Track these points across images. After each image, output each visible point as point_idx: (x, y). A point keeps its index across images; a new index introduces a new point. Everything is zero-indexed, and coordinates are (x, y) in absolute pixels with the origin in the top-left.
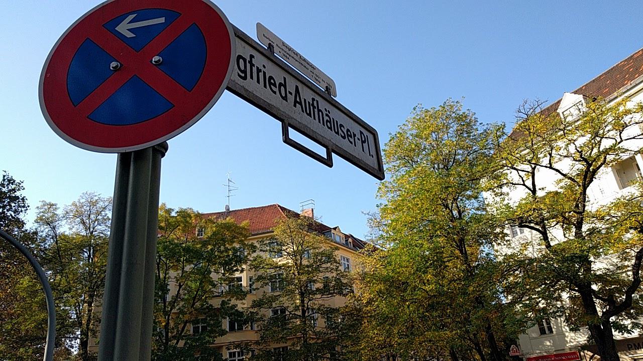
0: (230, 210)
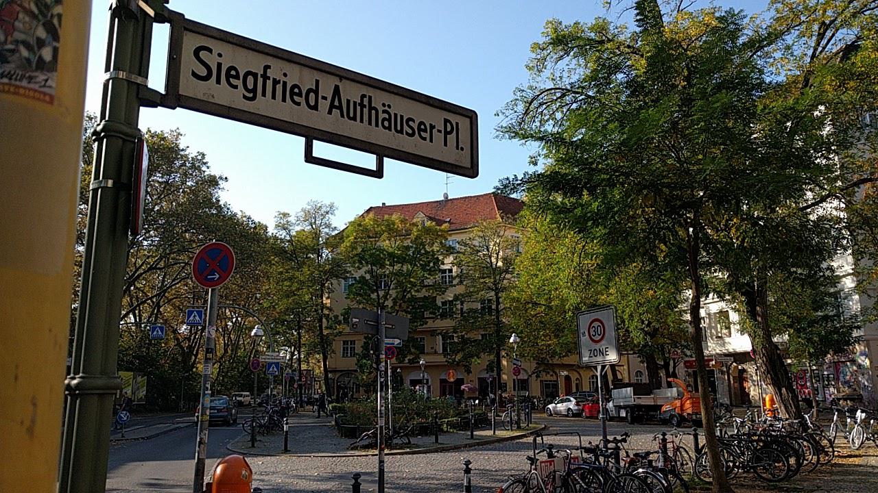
0: (449, 198)
